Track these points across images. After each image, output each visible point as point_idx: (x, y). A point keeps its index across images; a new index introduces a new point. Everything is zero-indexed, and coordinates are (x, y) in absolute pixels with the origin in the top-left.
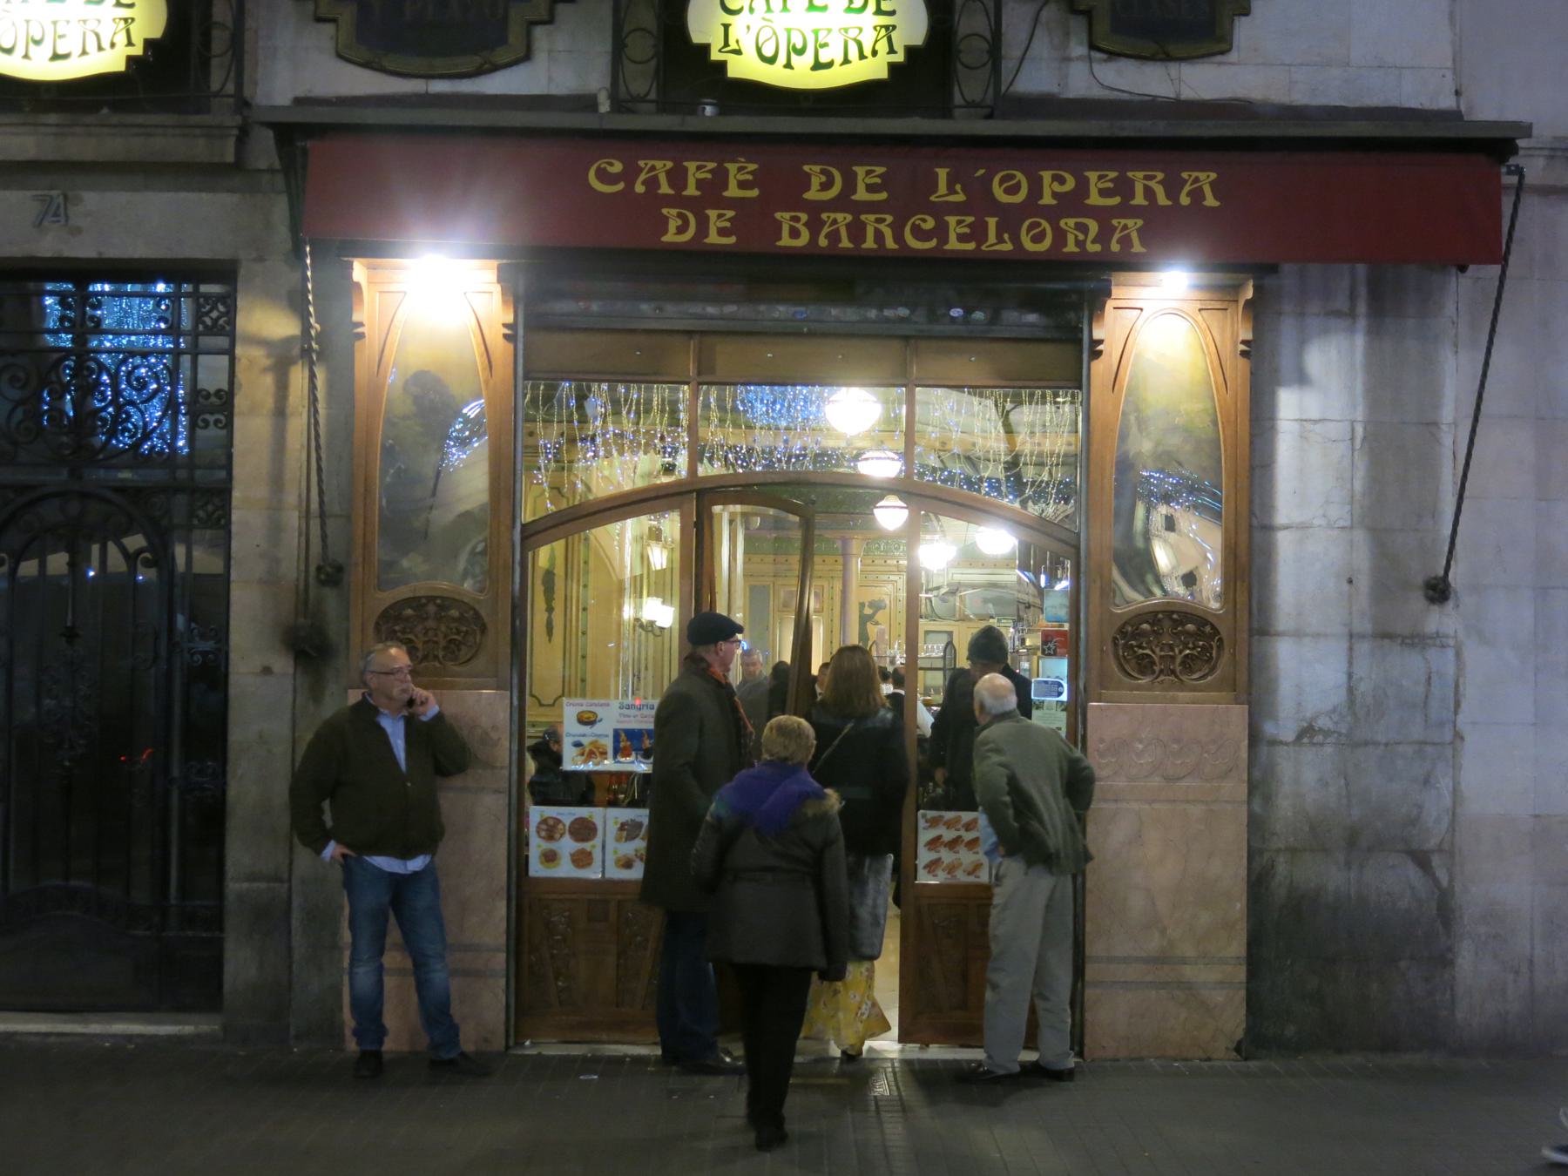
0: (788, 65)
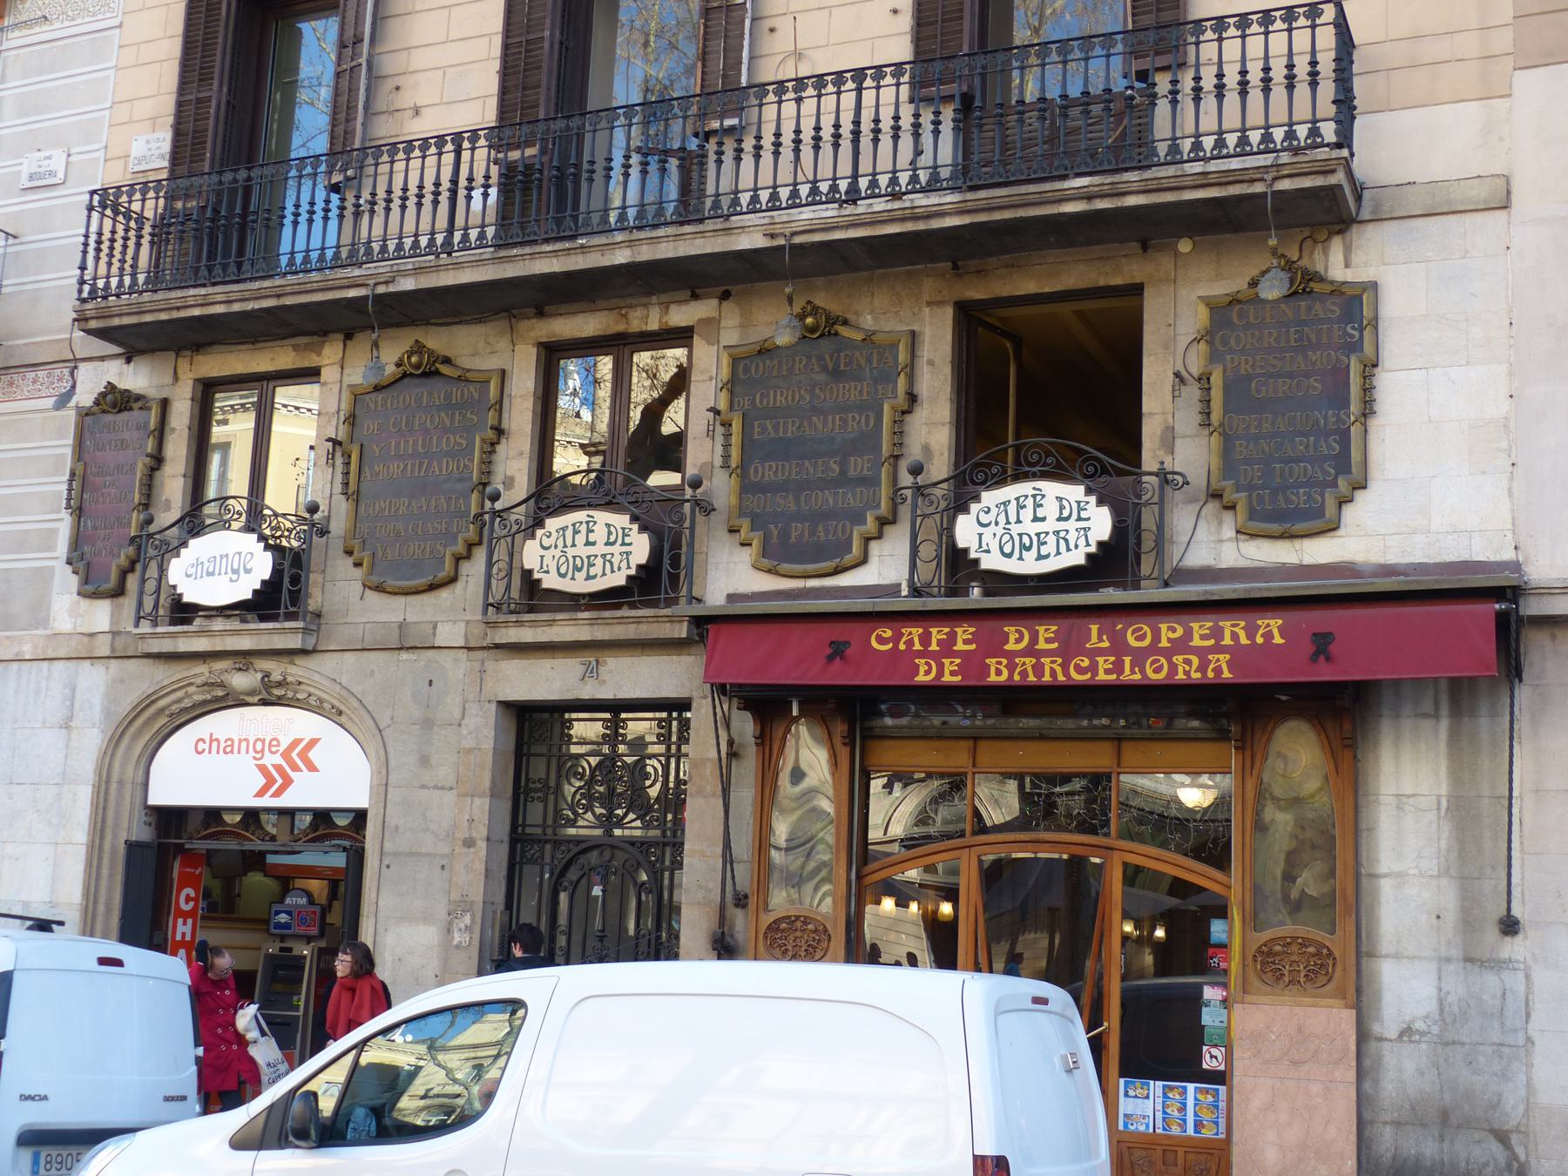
0: (1021, 558)
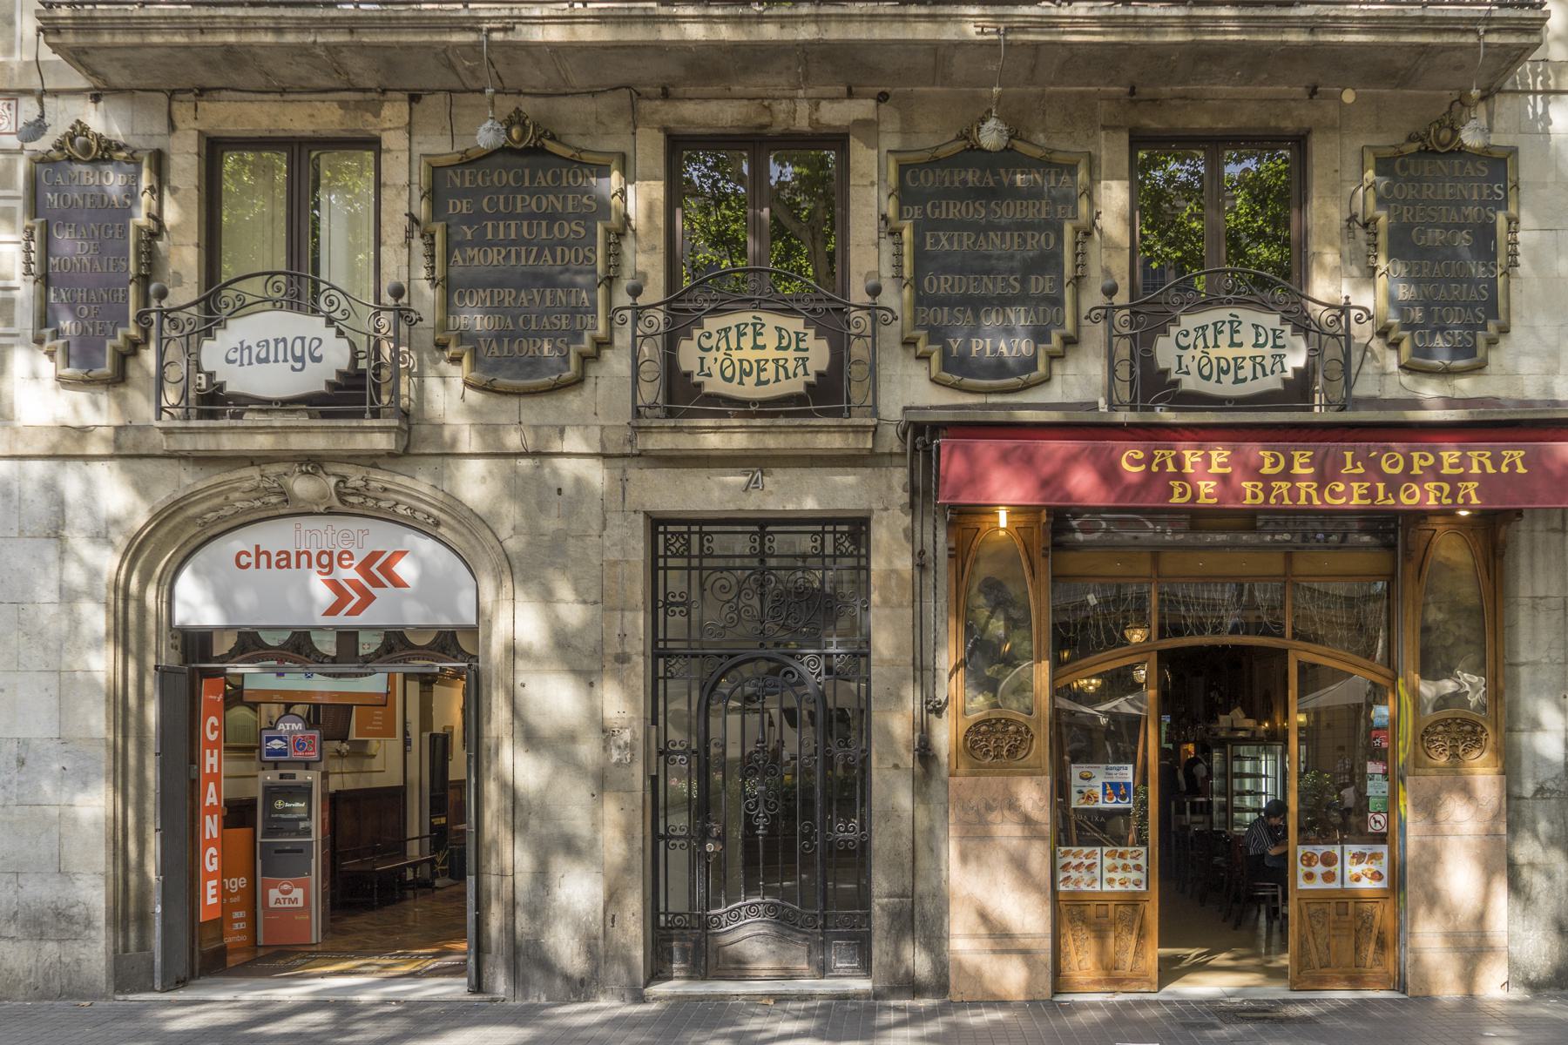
0: (1219, 381)
